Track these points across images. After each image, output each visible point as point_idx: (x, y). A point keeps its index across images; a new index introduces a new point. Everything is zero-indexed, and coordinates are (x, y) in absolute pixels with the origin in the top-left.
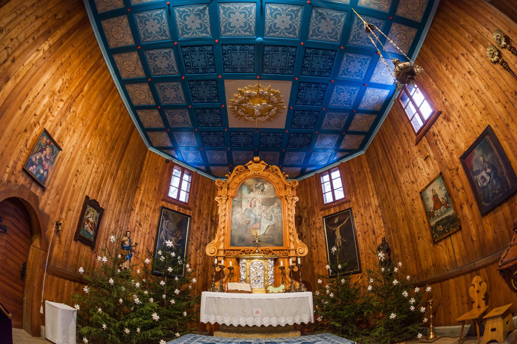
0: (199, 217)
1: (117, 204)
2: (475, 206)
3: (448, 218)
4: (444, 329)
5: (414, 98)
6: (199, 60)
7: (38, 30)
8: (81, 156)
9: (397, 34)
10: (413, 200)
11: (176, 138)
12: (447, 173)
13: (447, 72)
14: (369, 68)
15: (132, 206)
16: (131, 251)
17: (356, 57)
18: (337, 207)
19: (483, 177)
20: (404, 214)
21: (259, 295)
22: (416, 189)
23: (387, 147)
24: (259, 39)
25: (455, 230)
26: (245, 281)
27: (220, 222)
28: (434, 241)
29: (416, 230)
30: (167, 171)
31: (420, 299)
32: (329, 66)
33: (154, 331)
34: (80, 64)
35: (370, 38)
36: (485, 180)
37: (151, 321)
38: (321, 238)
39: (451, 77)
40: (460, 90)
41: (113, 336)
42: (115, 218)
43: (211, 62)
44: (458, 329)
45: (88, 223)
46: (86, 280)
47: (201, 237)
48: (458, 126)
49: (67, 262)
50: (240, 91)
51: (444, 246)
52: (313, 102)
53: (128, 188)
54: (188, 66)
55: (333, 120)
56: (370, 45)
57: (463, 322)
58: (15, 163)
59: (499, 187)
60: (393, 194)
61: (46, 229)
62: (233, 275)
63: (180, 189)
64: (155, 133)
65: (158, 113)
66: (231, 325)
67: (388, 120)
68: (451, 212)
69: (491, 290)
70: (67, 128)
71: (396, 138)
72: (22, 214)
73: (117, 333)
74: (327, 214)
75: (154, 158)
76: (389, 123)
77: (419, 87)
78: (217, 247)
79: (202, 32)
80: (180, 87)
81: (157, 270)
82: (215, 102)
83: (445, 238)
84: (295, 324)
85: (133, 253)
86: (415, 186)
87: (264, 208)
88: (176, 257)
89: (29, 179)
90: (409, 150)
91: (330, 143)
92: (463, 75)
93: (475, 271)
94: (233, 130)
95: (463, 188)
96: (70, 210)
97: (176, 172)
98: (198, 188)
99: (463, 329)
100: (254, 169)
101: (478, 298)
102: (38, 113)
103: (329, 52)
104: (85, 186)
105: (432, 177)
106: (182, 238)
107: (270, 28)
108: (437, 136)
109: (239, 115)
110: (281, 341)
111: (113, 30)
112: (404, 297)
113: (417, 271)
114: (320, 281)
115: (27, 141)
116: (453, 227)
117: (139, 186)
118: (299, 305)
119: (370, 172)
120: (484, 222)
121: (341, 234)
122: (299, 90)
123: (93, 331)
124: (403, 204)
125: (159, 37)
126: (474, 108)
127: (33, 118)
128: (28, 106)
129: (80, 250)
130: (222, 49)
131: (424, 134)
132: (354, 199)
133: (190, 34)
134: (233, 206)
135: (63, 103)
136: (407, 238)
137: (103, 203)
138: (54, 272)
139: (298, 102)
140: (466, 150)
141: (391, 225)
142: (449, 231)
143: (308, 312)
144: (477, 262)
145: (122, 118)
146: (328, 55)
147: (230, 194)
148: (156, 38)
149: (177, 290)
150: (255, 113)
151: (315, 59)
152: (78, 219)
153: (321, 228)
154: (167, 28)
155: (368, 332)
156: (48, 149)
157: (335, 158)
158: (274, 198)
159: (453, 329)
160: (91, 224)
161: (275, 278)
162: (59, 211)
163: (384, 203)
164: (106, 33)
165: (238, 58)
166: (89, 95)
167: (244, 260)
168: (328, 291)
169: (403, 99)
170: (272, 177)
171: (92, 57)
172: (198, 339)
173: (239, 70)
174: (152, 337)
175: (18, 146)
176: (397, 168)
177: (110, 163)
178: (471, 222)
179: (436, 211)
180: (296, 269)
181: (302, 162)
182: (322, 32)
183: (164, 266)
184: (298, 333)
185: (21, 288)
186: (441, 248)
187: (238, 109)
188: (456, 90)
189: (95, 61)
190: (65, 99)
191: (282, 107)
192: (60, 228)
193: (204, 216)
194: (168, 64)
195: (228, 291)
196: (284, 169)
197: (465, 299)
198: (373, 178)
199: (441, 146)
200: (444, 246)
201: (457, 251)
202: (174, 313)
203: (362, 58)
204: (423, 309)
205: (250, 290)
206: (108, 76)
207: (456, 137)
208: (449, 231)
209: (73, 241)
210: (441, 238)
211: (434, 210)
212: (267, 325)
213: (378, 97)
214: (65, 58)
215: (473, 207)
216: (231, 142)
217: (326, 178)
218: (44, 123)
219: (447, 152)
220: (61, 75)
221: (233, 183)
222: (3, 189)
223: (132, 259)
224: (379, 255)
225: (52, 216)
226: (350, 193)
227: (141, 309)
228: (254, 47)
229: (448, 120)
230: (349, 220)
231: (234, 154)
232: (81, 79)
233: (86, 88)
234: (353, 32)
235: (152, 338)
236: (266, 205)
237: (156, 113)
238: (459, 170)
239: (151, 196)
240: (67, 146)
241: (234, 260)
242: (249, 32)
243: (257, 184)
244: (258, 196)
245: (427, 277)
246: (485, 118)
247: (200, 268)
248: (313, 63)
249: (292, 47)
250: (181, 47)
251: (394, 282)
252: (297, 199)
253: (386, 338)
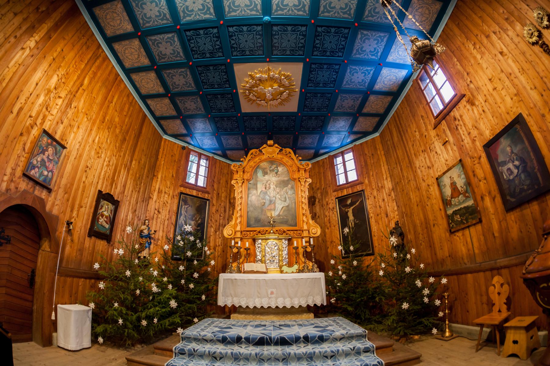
0: (217, 200)
1: (133, 194)
2: (498, 199)
3: (466, 208)
4: (461, 328)
5: (435, 78)
6: (205, 44)
7: (19, 27)
8: (90, 151)
9: (419, 8)
10: (428, 185)
11: (190, 125)
12: (468, 161)
13: (475, 52)
14: (385, 46)
15: (149, 195)
16: (150, 239)
17: (372, 35)
18: (350, 189)
19: (509, 169)
20: (418, 200)
21: (274, 275)
22: (432, 175)
23: (403, 130)
24: (267, 18)
25: (474, 222)
26: (261, 261)
27: (236, 205)
28: (450, 231)
29: (431, 217)
30: (184, 158)
31: (435, 290)
32: (342, 45)
33: (171, 319)
34: (75, 56)
35: (387, 13)
36: (512, 173)
37: (169, 309)
38: (334, 218)
39: (479, 56)
40: (489, 72)
41: (130, 331)
42: (132, 208)
43: (218, 45)
44: (476, 331)
45: (102, 217)
46: (102, 275)
47: (220, 219)
48: (484, 111)
49: (81, 261)
50: (250, 75)
51: (461, 238)
52: (325, 84)
53: (144, 178)
54: (194, 51)
55: (346, 102)
56: (387, 21)
57: (482, 326)
58: (13, 169)
59: (528, 182)
60: (407, 178)
61: (55, 230)
63: (197, 174)
64: (168, 121)
65: (169, 101)
66: (247, 307)
67: (405, 102)
68: (470, 203)
69: (514, 294)
70: (70, 125)
71: (413, 121)
72: (28, 221)
73: (135, 326)
74: (340, 196)
75: (169, 145)
76: (406, 104)
77: (440, 67)
78: (234, 228)
79: (205, 14)
80: (188, 73)
81: (176, 255)
82: (226, 88)
83: (463, 229)
84: (308, 306)
85: (152, 241)
86: (431, 171)
87: (278, 190)
88: (195, 241)
89: (31, 183)
90: (427, 134)
91: (344, 126)
92: (494, 56)
93: (496, 270)
94: (247, 114)
95: (485, 179)
96: (82, 207)
97: (192, 157)
98: (215, 172)
99: (481, 333)
100: (268, 153)
101: (499, 302)
102: (34, 114)
103: (342, 30)
104: (97, 181)
105: (451, 164)
106: (202, 221)
107: (277, 5)
108: (459, 120)
109: (251, 100)
110: (294, 323)
111: (108, 17)
112: (417, 286)
113: (432, 259)
114: (332, 262)
115: (25, 144)
116: (473, 219)
117: (155, 174)
119: (385, 154)
120: (508, 218)
121: (353, 216)
122: (311, 72)
123: (108, 329)
124: (418, 188)
125: (160, 21)
126: (503, 93)
127: (29, 120)
128: (21, 109)
129: (95, 245)
130: (228, 31)
131: (444, 118)
132: (367, 181)
133: (193, 16)
134: (249, 189)
135: (61, 100)
136: (422, 224)
137: (118, 195)
138: (66, 273)
139: (310, 85)
140: (491, 138)
141: (405, 210)
142: (467, 222)
143: (321, 293)
144: (498, 261)
145: (131, 108)
146: (341, 33)
147: (245, 177)
148: (156, 23)
149: (196, 273)
150: (267, 97)
151: (327, 38)
152: (91, 214)
153: (334, 208)
154: (166, 11)
155: (380, 319)
156: (50, 149)
157: (349, 140)
158: (288, 181)
159: (472, 330)
160: (106, 217)
161: (289, 258)
162: (69, 209)
163: (398, 186)
164: (100, 21)
165: (247, 40)
166: (90, 88)
167: (260, 241)
168: (340, 273)
169: (422, 79)
170: (286, 159)
171: (88, 48)
172: (215, 324)
173: (248, 53)
174: (169, 325)
175: (15, 152)
176: (413, 152)
177: (122, 155)
178: (493, 216)
179: (453, 199)
180: (309, 249)
181: (316, 144)
182: (334, 7)
183: (183, 250)
184: (312, 315)
185: (29, 297)
186: (458, 238)
187: (250, 93)
188: (484, 72)
189: (93, 52)
190: (63, 95)
191: (293, 90)
192: (71, 227)
193: (223, 199)
194: (173, 50)
195: (244, 272)
196: (298, 151)
197: (485, 299)
198: (386, 161)
199: (462, 131)
200: (461, 238)
201: (476, 245)
202: (193, 298)
203: (378, 35)
204: (438, 302)
205: (265, 270)
206: (110, 67)
207: (480, 123)
208: (467, 222)
209: (87, 237)
210: (459, 228)
211: (452, 198)
212: (281, 306)
213: (394, 78)
214: (57, 53)
215: (496, 200)
216: (245, 127)
217: (339, 160)
218: (42, 124)
219: (468, 139)
220: (55, 71)
221: (248, 167)
222: (1, 199)
223: (152, 246)
224: (392, 239)
225: (61, 216)
226: (363, 175)
227: (159, 298)
228: (262, 28)
229: (472, 104)
230: (362, 201)
231: (248, 138)
232: (79, 72)
233: (86, 82)
234: (368, 6)
235: (169, 327)
236: (280, 187)
237: (167, 101)
238: (482, 159)
239: (168, 183)
240: (72, 143)
241: (250, 240)
242: (255, 11)
243: (271, 167)
244: (272, 179)
245: (442, 267)
246: (517, 105)
247: (219, 249)
248: (325, 42)
249: (302, 26)
250: (185, 31)
251: (406, 269)
252: (310, 180)
253: (399, 329)
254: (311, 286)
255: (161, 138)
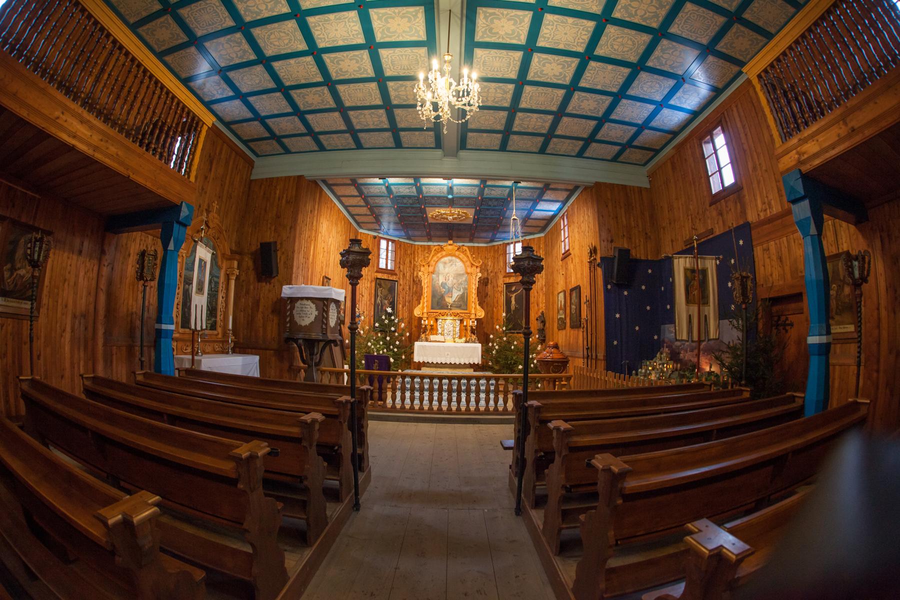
21: (450, 344)
24: (450, 197)
62: (433, 330)
118: (473, 352)
179: (776, 209)
217: (512, 246)
254: (473, 352)
255: (357, 232)
